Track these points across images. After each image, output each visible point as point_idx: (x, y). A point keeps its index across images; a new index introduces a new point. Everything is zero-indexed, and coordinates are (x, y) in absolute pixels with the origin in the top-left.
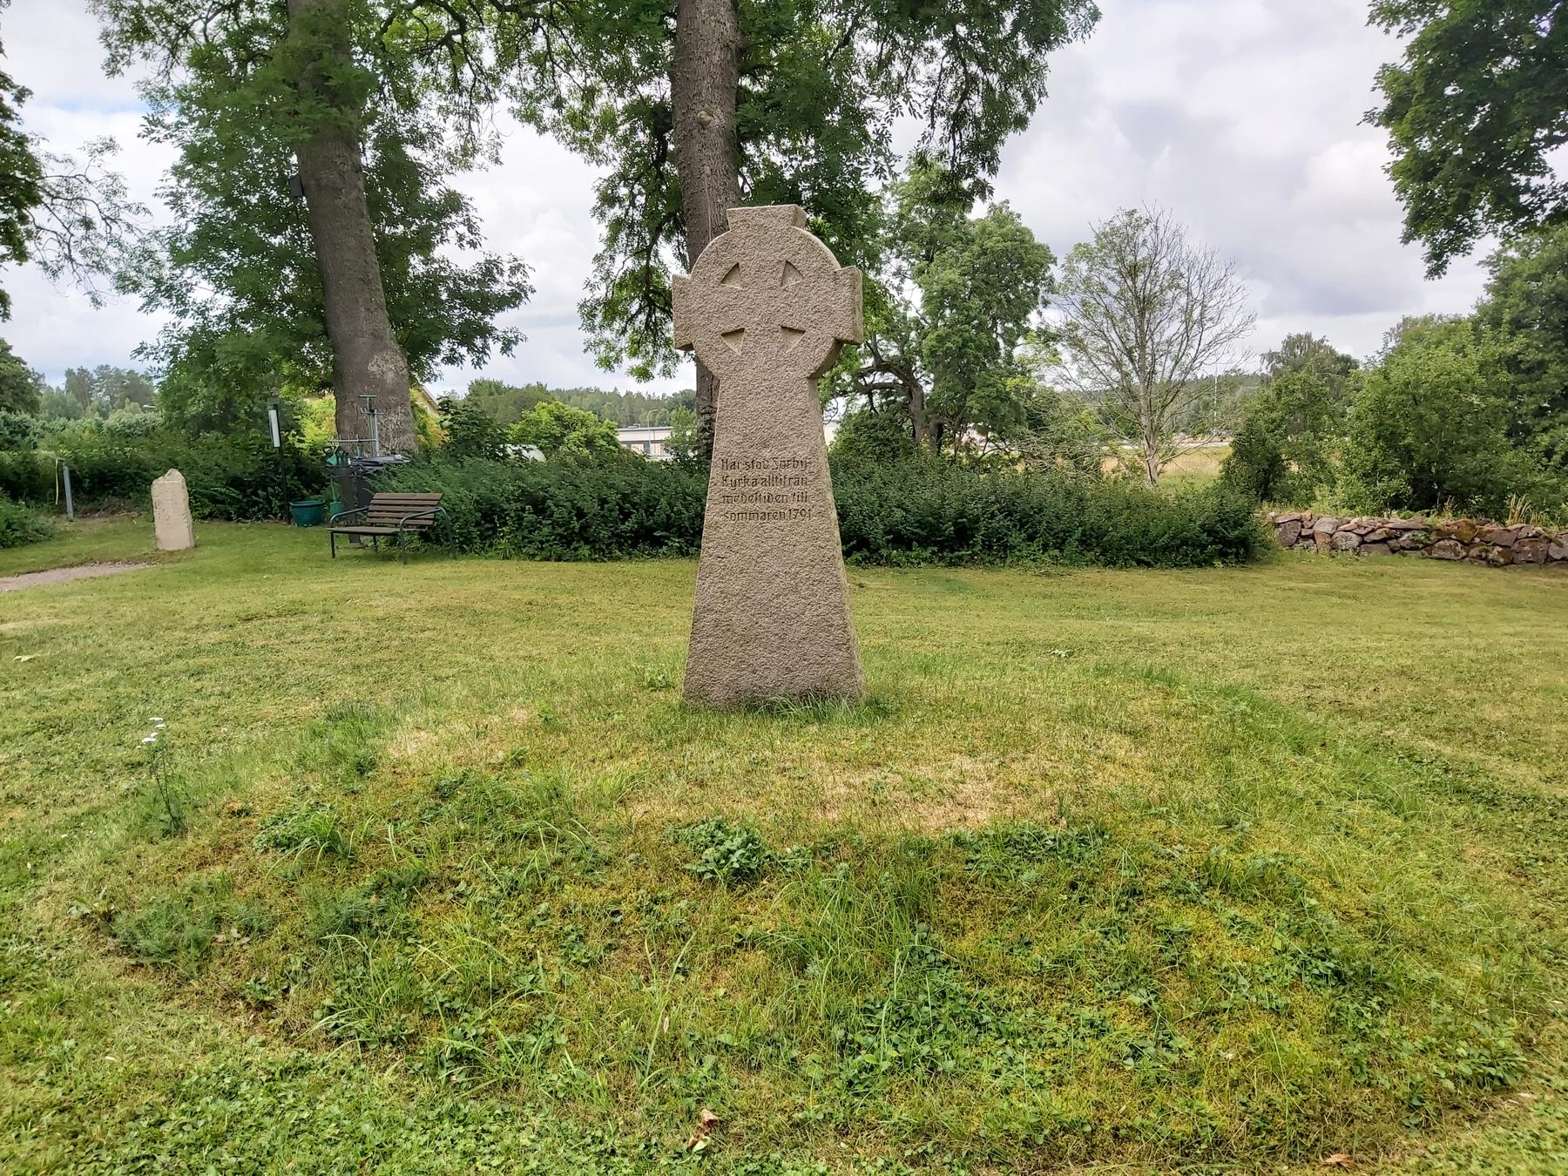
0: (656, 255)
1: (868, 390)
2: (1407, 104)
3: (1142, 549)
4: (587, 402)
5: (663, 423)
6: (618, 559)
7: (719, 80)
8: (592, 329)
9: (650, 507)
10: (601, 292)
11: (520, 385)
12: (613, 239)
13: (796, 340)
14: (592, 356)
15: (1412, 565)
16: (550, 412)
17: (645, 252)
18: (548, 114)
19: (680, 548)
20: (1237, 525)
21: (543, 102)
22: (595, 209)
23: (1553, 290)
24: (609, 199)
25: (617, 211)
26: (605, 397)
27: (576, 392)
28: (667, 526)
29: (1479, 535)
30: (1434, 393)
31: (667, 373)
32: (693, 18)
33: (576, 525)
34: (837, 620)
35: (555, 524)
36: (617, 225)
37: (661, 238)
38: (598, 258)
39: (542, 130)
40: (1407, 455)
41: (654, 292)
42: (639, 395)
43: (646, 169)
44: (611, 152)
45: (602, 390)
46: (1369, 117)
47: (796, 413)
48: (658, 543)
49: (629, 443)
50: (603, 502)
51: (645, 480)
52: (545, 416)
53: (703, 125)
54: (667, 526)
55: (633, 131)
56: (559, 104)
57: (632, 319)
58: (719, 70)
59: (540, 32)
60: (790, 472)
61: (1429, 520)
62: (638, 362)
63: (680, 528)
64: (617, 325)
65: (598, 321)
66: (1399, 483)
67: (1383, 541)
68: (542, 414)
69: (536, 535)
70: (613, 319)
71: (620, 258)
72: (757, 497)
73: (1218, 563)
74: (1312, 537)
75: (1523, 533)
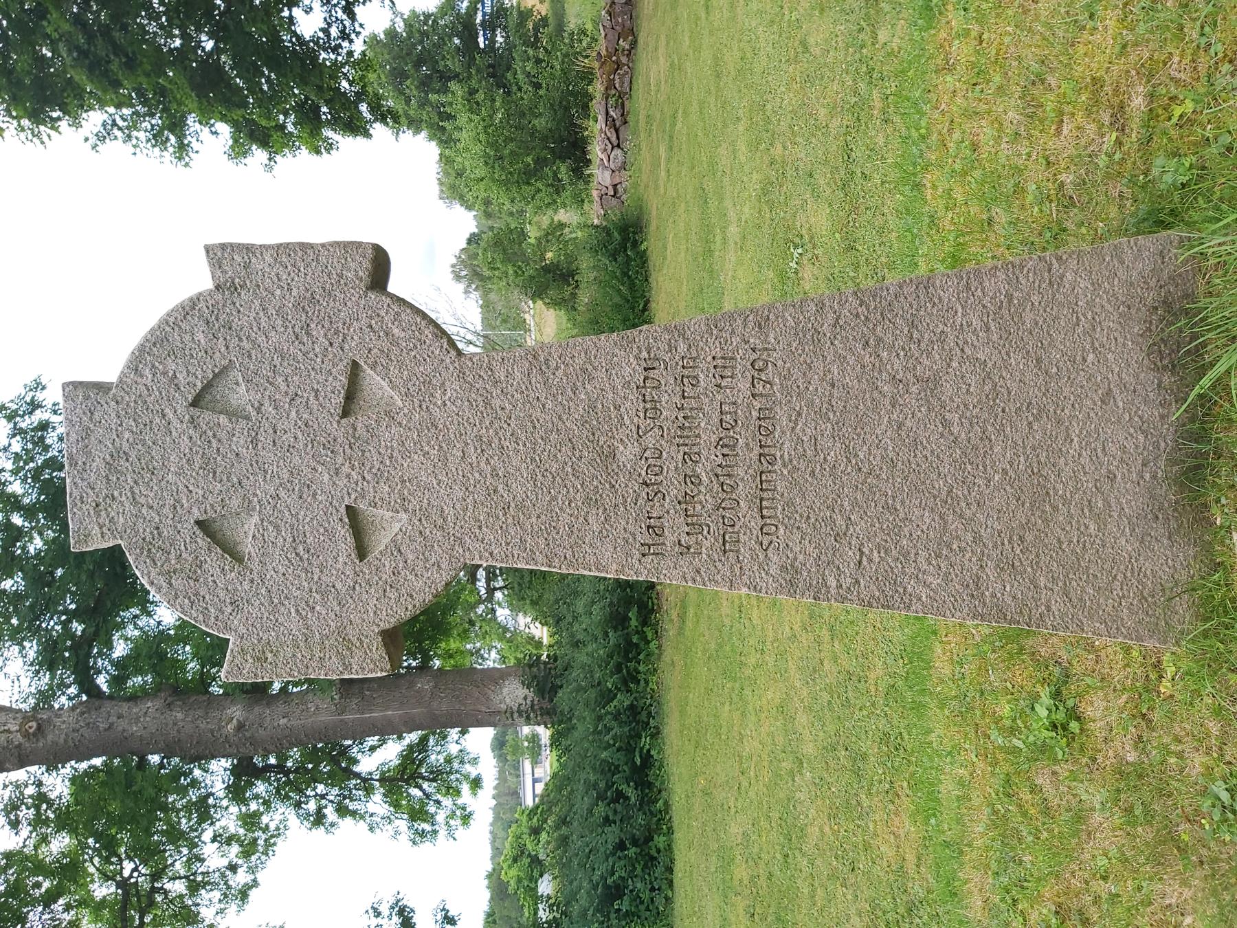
0: (371, 774)
1: (491, 591)
2: (257, 135)
3: (633, 308)
4: (501, 834)
5: (517, 767)
6: (666, 803)
7: (200, 712)
8: (435, 832)
9: (610, 769)
10: (402, 824)
11: (487, 895)
12: (354, 814)
13: (376, 384)
14: (461, 832)
15: (639, 105)
16: (510, 867)
17: (366, 785)
18: (242, 877)
19: (653, 736)
20: (609, 234)
21: (231, 883)
22: (328, 832)
23: (417, 88)
24: (318, 819)
25: (330, 812)
26: (497, 818)
27: (493, 842)
28: (629, 750)
29: (610, 58)
30: (493, 145)
31: (474, 762)
32: (141, 738)
33: (632, 852)
34: (997, 284)
35: (632, 875)
36: (342, 811)
37: (357, 769)
38: (371, 829)
39: (255, 884)
40: (540, 162)
41: (402, 775)
42: (495, 788)
43: (293, 785)
44: (278, 817)
45: (491, 820)
46: (269, 168)
47: (536, 377)
48: (647, 759)
49: (535, 796)
50: (607, 821)
51: (583, 776)
52: (513, 872)
53: (240, 727)
54: (629, 750)
55: (257, 797)
56: (233, 868)
57: (428, 796)
58: (191, 712)
59: (168, 886)
60: (668, 401)
61: (598, 95)
62: (465, 788)
63: (631, 737)
64: (432, 809)
65: (427, 827)
66: (564, 170)
67: (617, 131)
68: (511, 875)
69: (645, 896)
70: (427, 812)
71: (371, 807)
72: (723, 475)
73: (643, 248)
74: (615, 186)
75: (608, 24)
